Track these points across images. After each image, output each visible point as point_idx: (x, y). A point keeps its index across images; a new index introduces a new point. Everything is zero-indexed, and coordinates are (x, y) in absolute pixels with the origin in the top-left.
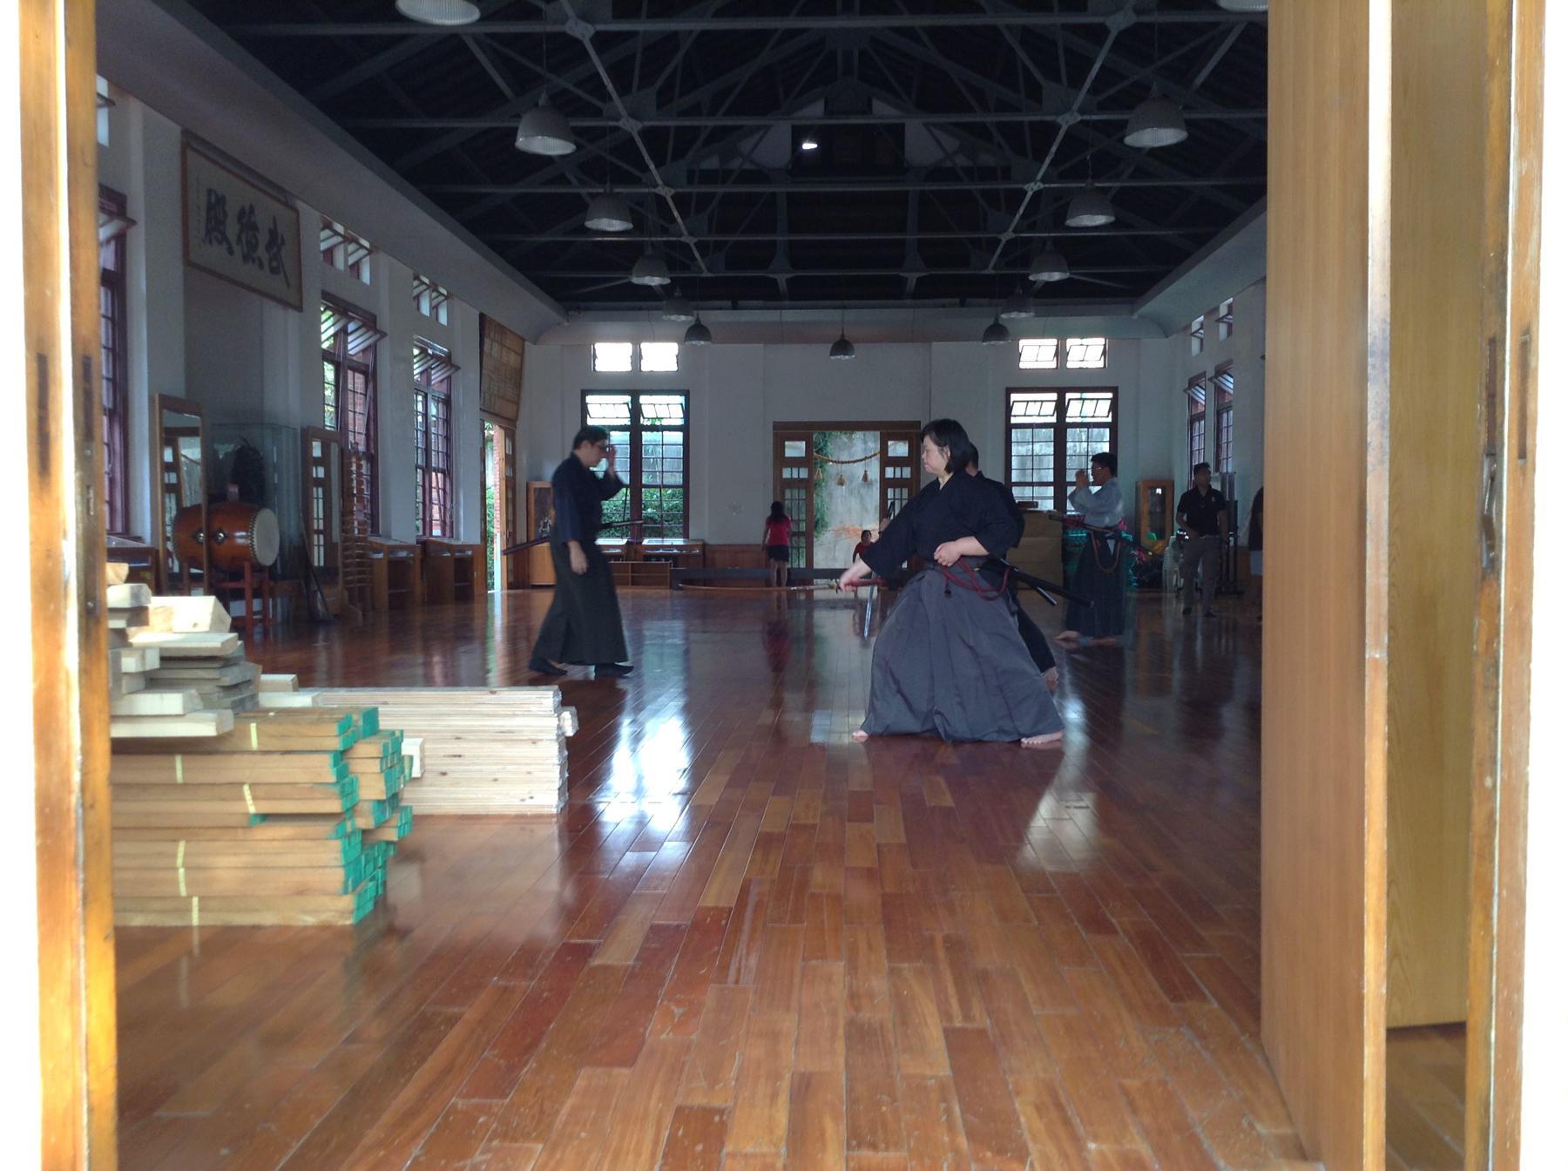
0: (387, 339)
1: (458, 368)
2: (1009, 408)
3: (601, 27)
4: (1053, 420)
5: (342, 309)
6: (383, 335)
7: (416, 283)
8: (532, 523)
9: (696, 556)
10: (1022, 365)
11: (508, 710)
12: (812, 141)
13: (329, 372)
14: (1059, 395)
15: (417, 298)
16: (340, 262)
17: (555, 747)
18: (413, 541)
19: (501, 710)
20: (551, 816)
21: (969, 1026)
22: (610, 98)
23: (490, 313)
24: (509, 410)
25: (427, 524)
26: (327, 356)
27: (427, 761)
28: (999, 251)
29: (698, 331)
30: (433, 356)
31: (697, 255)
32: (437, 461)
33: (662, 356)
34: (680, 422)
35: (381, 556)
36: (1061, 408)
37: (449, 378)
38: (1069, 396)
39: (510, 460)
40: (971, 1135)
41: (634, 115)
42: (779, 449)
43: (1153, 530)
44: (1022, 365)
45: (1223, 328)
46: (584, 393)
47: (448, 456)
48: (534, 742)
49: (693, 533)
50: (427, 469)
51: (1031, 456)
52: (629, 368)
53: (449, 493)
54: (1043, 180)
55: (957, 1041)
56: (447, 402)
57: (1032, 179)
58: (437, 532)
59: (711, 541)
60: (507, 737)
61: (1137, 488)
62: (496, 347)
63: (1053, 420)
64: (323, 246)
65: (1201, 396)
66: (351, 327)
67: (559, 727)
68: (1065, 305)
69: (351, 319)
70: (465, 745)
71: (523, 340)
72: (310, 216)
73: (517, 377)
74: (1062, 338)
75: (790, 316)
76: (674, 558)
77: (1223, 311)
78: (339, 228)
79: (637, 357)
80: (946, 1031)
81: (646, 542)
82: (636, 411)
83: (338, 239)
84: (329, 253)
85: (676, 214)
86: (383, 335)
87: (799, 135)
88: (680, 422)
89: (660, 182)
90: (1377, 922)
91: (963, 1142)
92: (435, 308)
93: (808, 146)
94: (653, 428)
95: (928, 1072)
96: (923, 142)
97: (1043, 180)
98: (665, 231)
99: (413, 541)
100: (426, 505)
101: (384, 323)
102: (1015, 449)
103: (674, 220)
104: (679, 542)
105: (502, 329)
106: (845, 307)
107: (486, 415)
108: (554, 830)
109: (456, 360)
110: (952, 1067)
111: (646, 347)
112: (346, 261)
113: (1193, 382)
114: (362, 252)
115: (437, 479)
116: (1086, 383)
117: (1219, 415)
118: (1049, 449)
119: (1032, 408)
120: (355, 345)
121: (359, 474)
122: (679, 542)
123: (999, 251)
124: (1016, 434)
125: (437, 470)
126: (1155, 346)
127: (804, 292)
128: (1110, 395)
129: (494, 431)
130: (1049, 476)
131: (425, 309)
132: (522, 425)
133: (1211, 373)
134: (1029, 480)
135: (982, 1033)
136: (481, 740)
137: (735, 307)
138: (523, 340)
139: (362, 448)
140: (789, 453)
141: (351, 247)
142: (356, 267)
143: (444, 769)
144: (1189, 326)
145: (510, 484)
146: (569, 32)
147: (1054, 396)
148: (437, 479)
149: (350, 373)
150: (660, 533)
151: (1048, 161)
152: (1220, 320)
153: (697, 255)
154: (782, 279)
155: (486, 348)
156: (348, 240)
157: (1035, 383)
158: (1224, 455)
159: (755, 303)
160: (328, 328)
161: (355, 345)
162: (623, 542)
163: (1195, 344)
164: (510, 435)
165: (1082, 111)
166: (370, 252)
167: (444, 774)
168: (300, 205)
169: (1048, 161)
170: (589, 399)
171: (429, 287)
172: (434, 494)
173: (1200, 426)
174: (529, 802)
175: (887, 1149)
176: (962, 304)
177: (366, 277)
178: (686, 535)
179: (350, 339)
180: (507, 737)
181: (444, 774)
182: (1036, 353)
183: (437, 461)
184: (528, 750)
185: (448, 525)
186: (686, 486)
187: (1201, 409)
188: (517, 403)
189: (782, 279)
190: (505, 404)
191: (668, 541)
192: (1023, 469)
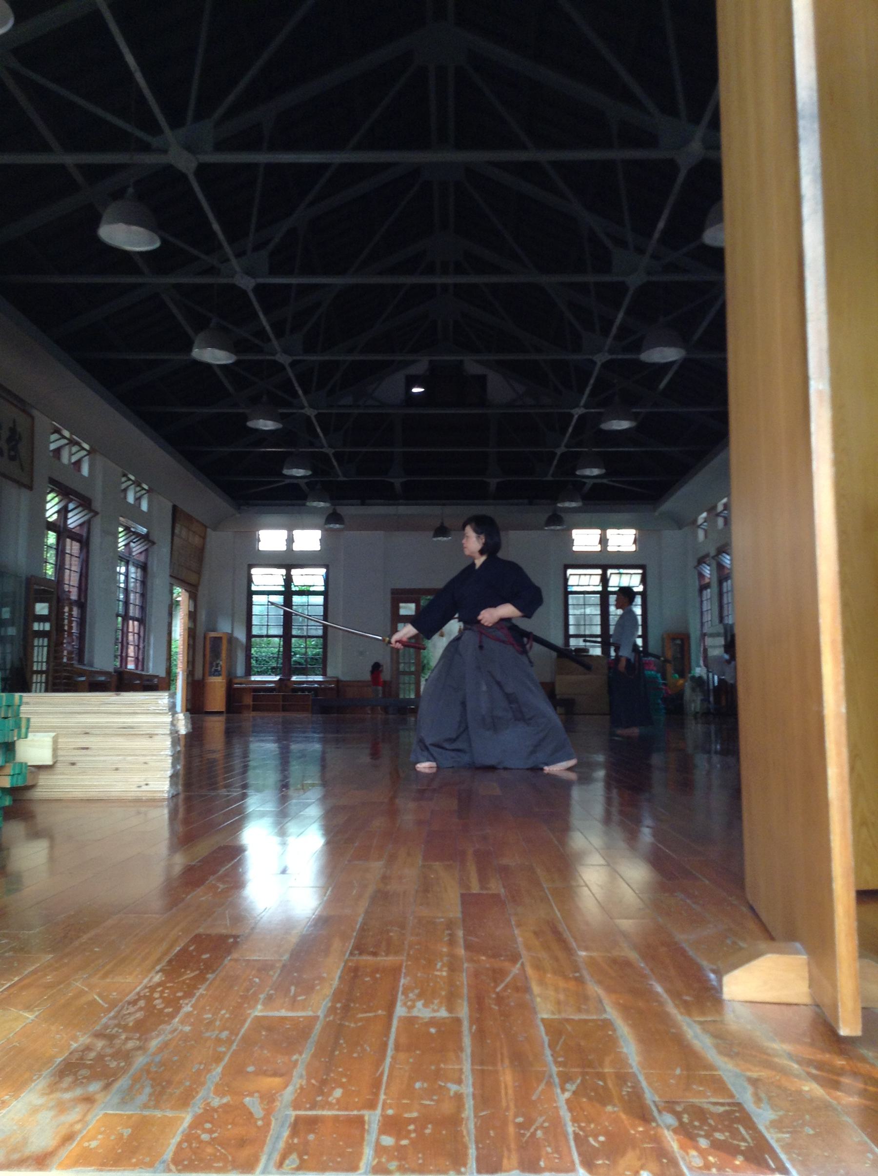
0: (99, 517)
1: (153, 543)
2: (566, 580)
3: (261, 280)
4: (600, 589)
5: (65, 492)
6: (96, 513)
7: (124, 479)
8: (207, 666)
9: (332, 689)
10: (575, 549)
11: (131, 710)
12: (420, 386)
13: (51, 538)
14: (599, 560)
15: (125, 490)
16: (65, 459)
17: (168, 743)
18: (111, 670)
19: (124, 709)
20: (163, 800)
21: (485, 892)
22: (269, 340)
23: (180, 506)
24: (193, 578)
25: (124, 659)
26: (51, 526)
27: (60, 753)
28: (555, 462)
29: (333, 517)
30: (134, 533)
31: (335, 463)
32: (134, 611)
33: (309, 540)
34: (322, 589)
35: (83, 679)
36: (605, 580)
37: (146, 550)
38: (610, 571)
39: (192, 616)
40: (468, 947)
41: (286, 351)
42: (395, 609)
43: (676, 672)
44: (575, 549)
45: (720, 521)
46: (251, 566)
47: (143, 608)
48: (151, 736)
49: (330, 672)
50: (126, 617)
51: (584, 617)
52: (284, 548)
53: (143, 637)
54: (585, 407)
55: (467, 900)
56: (144, 567)
57: (577, 406)
58: (131, 666)
59: (342, 678)
60: (128, 732)
61: (663, 639)
62: (184, 533)
63: (600, 589)
64: (53, 447)
65: (707, 571)
66: (71, 506)
67: (173, 724)
68: (603, 504)
69: (71, 501)
70: (92, 739)
71: (206, 527)
72: (42, 421)
73: (200, 554)
74: (604, 529)
75: (403, 510)
76: (316, 691)
77: (720, 508)
78: (66, 433)
79: (290, 541)
80: (462, 895)
81: (294, 678)
82: (288, 580)
83: (65, 441)
84: (58, 451)
85: (319, 430)
86: (96, 513)
87: (413, 381)
88: (322, 589)
89: (306, 404)
90: (833, 642)
91: (461, 951)
92: (138, 499)
93: (416, 390)
94: (301, 593)
95: (440, 915)
96: (500, 389)
97: (586, 406)
98: (312, 445)
99: (111, 670)
100: (124, 645)
101: (97, 505)
102: (571, 612)
103: (318, 436)
104: (319, 678)
105: (189, 518)
106: (444, 505)
107: (173, 581)
108: (164, 813)
109: (154, 537)
110: (462, 912)
111: (297, 533)
112: (70, 459)
113: (701, 561)
114: (84, 453)
115: (133, 626)
116: (622, 562)
117: (720, 583)
118: (597, 611)
119: (582, 580)
120: (74, 520)
121: (71, 615)
122: (319, 678)
123: (555, 462)
124: (572, 599)
125: (134, 619)
126: (671, 536)
127: (414, 493)
128: (640, 571)
129: (180, 594)
130: (597, 630)
131: (131, 499)
132: (202, 591)
133: (713, 552)
134: (582, 633)
135: (496, 896)
136: (105, 735)
137: (363, 504)
138: (206, 527)
139: (74, 596)
140: (402, 612)
141: (74, 449)
142: (78, 463)
143: (74, 759)
144: (695, 520)
145: (191, 634)
146: (237, 283)
147: (599, 571)
148: (133, 626)
149: (68, 541)
150: (303, 672)
151: (587, 391)
152: (718, 515)
153: (335, 463)
154: (397, 482)
155: (177, 531)
156: (72, 442)
157: (585, 562)
158: (725, 613)
159: (379, 501)
160: (52, 507)
161: (74, 520)
162: (277, 678)
163: (701, 534)
164: (193, 596)
165: (611, 352)
166: (89, 453)
167: (73, 764)
168: (35, 413)
169: (587, 391)
170: (254, 571)
171: (134, 482)
172: (131, 637)
173: (707, 593)
174: (144, 788)
175: (387, 955)
176: (530, 504)
177: (85, 470)
178: (324, 674)
179: (70, 515)
180: (128, 732)
181: (73, 764)
182: (585, 540)
183: (134, 611)
184: (145, 743)
185: (140, 661)
186: (325, 636)
187: (707, 581)
188: (199, 573)
189: (397, 482)
190: (190, 572)
191: (311, 678)
192: (577, 625)
